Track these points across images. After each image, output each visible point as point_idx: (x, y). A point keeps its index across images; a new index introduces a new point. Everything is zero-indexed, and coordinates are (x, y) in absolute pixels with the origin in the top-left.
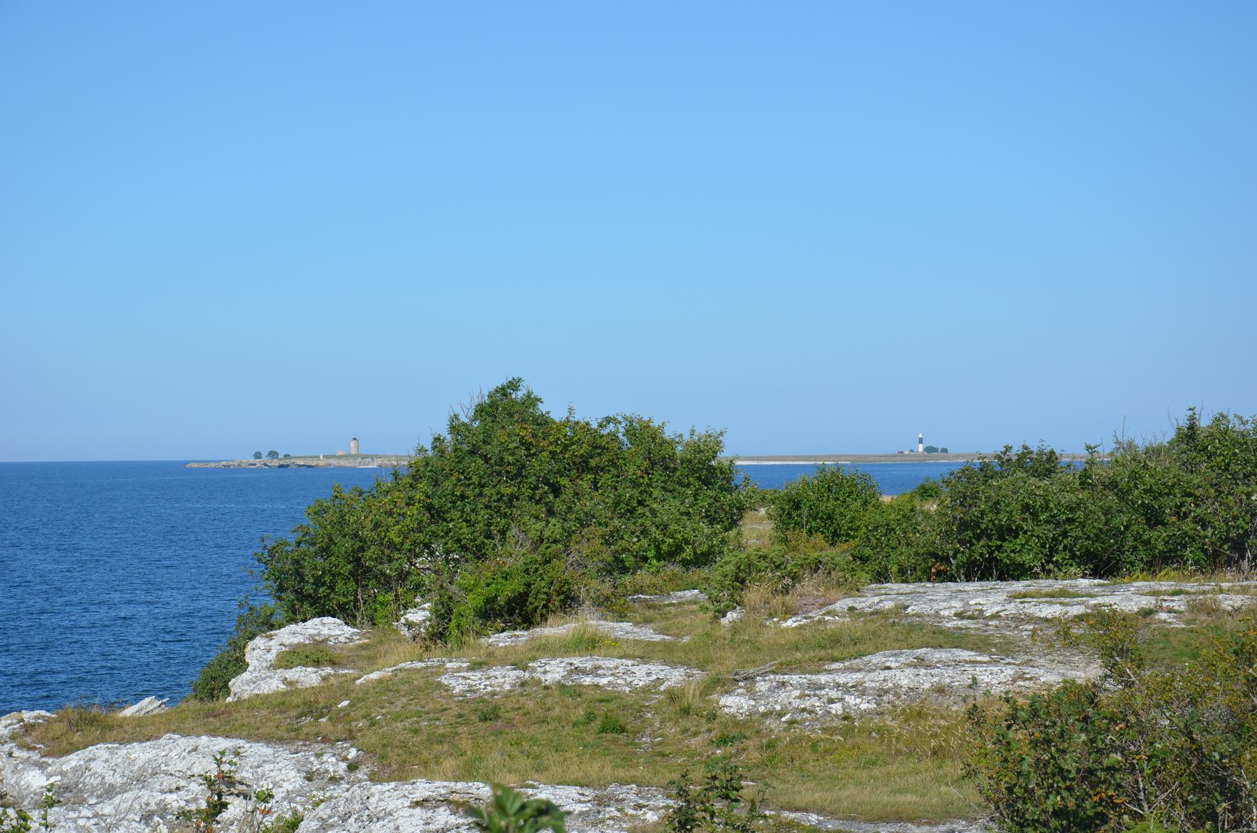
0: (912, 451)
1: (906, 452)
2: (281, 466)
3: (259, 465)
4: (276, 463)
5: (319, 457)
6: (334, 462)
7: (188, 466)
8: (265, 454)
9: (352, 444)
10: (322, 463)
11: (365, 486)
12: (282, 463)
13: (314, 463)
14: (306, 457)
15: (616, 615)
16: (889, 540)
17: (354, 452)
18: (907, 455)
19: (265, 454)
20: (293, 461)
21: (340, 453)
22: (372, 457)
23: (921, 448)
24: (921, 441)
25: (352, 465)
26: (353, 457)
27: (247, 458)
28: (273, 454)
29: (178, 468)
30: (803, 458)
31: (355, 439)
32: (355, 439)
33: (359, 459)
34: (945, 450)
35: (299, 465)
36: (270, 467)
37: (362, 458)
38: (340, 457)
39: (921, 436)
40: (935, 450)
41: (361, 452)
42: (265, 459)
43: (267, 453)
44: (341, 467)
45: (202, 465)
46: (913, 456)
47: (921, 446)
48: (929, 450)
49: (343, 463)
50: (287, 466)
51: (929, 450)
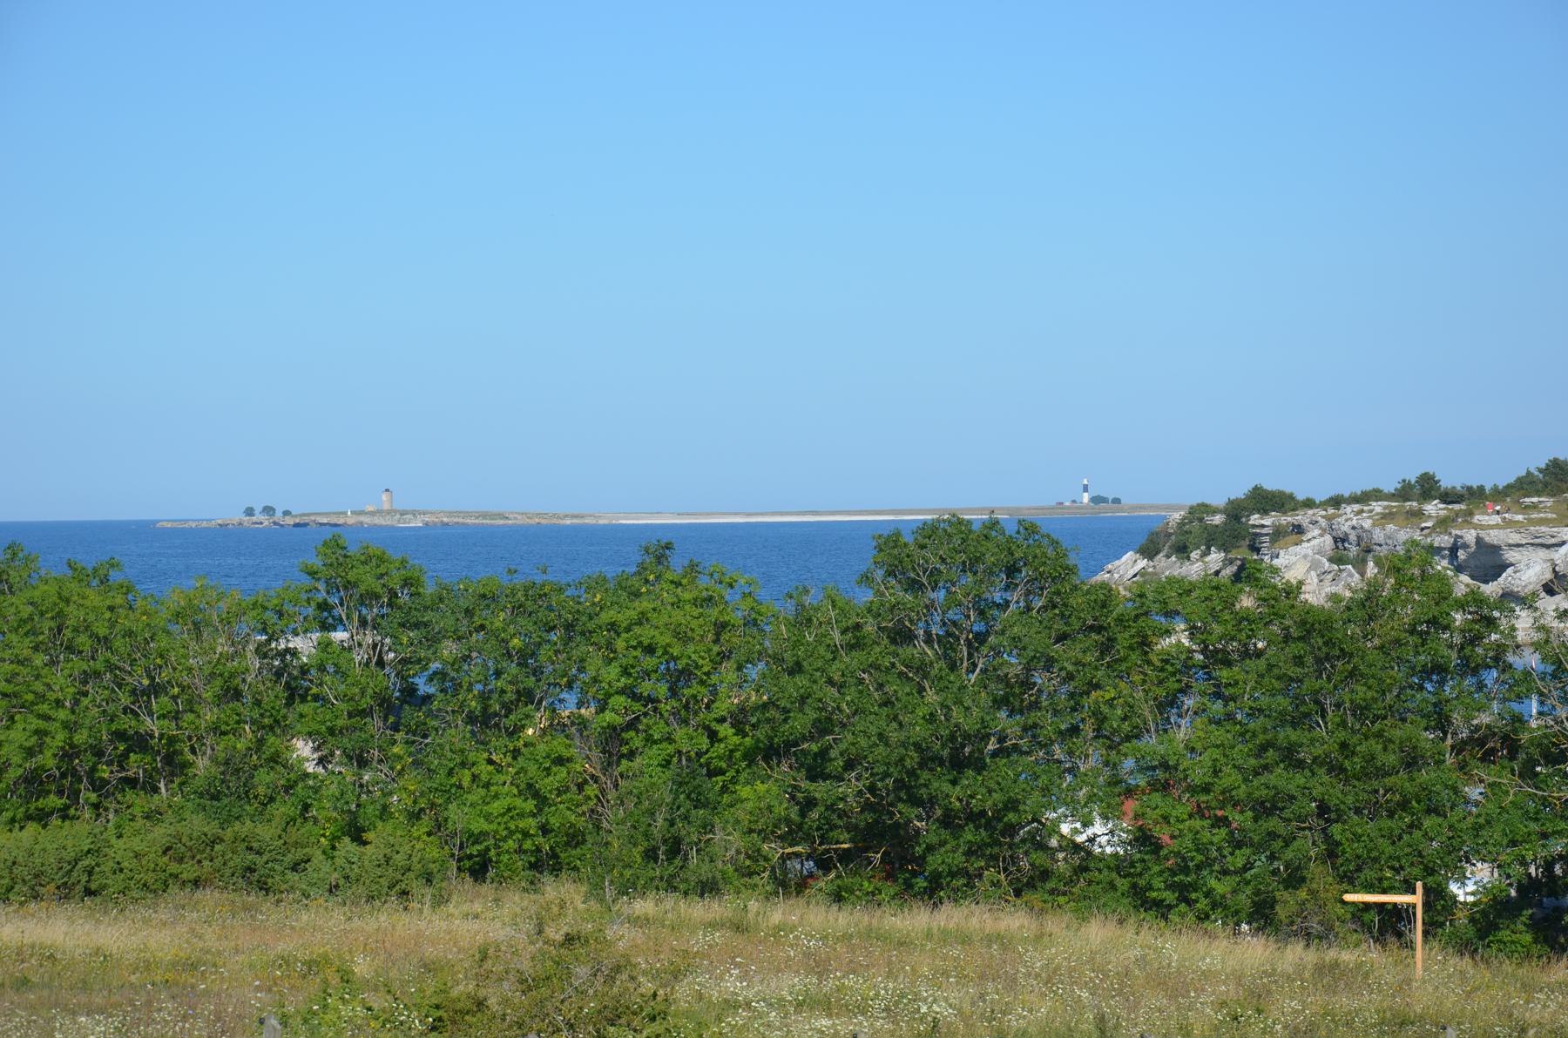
0: (1074, 501)
1: (1067, 504)
2: (297, 525)
3: (266, 523)
4: (290, 521)
5: (345, 513)
6: (366, 520)
7: (158, 525)
8: (258, 509)
9: (384, 497)
10: (351, 521)
11: (88, 561)
12: (297, 521)
13: (341, 521)
14: (330, 513)
15: (1153, 840)
16: (982, 997)
17: (386, 507)
18: (1069, 507)
19: (258, 509)
20: (313, 518)
21: (370, 508)
22: (414, 513)
23: (1086, 498)
24: (1086, 488)
25: (388, 523)
26: (389, 512)
27: (235, 516)
28: (269, 510)
29: (129, 523)
30: (782, 514)
31: (387, 490)
32: (387, 490)
33: (398, 516)
34: (1117, 501)
35: (321, 524)
36: (282, 526)
37: (402, 515)
38: (372, 514)
39: (1085, 482)
40: (1104, 500)
41: (397, 506)
42: (258, 517)
43: (261, 509)
44: (375, 525)
45: (175, 525)
46: (1077, 508)
47: (1086, 495)
48: (1097, 500)
49: (378, 520)
50: (305, 525)
51: (1097, 500)
